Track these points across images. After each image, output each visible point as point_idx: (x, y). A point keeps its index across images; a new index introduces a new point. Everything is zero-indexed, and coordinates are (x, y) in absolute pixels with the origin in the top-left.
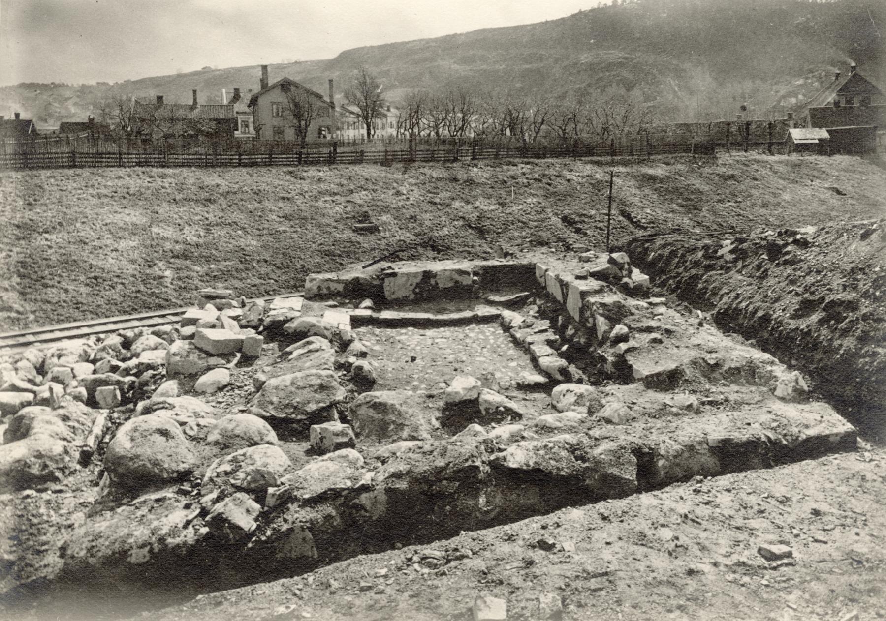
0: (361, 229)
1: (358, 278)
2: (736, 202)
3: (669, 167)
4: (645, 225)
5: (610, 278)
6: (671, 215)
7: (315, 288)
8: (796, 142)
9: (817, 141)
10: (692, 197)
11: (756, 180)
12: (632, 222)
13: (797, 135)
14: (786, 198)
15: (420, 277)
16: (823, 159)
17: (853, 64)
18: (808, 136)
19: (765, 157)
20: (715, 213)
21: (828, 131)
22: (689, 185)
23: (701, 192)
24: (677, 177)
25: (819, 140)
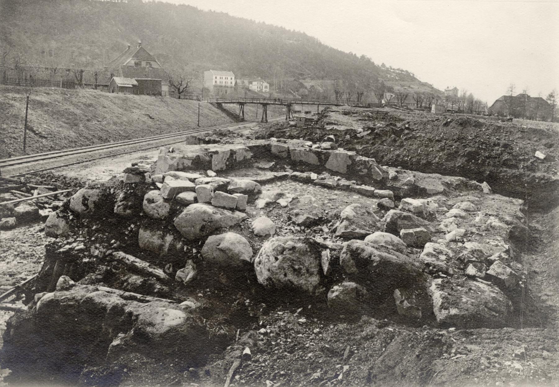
0: (335, 124)
1: (198, 156)
2: (98, 121)
3: (49, 97)
4: (46, 136)
5: (552, 126)
6: (60, 129)
7: (176, 164)
8: (119, 85)
9: (131, 86)
10: (71, 117)
11: (105, 107)
12: (36, 134)
13: (119, 81)
14: (125, 120)
15: (229, 154)
16: (136, 97)
17: (140, 42)
18: (126, 82)
19: (108, 94)
20: (87, 128)
21: (136, 80)
22: (66, 109)
23: (76, 114)
24: (57, 103)
25: (133, 85)
